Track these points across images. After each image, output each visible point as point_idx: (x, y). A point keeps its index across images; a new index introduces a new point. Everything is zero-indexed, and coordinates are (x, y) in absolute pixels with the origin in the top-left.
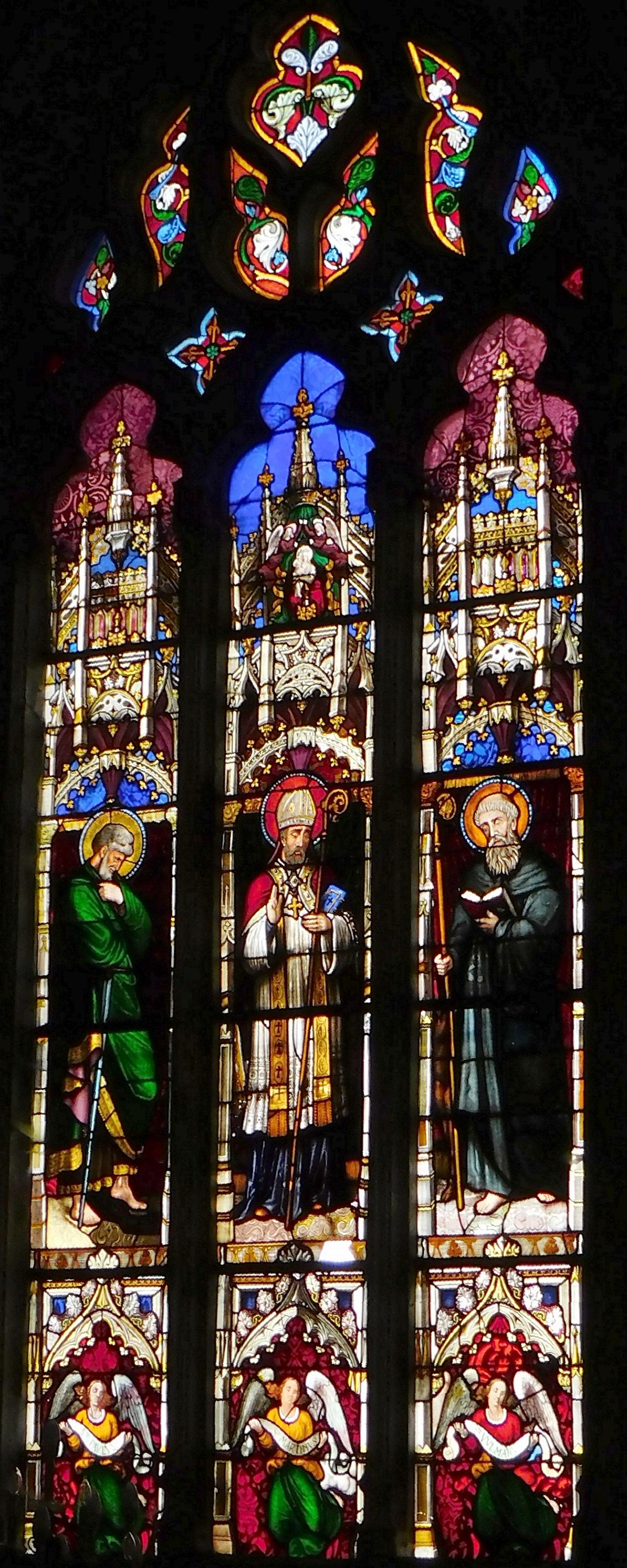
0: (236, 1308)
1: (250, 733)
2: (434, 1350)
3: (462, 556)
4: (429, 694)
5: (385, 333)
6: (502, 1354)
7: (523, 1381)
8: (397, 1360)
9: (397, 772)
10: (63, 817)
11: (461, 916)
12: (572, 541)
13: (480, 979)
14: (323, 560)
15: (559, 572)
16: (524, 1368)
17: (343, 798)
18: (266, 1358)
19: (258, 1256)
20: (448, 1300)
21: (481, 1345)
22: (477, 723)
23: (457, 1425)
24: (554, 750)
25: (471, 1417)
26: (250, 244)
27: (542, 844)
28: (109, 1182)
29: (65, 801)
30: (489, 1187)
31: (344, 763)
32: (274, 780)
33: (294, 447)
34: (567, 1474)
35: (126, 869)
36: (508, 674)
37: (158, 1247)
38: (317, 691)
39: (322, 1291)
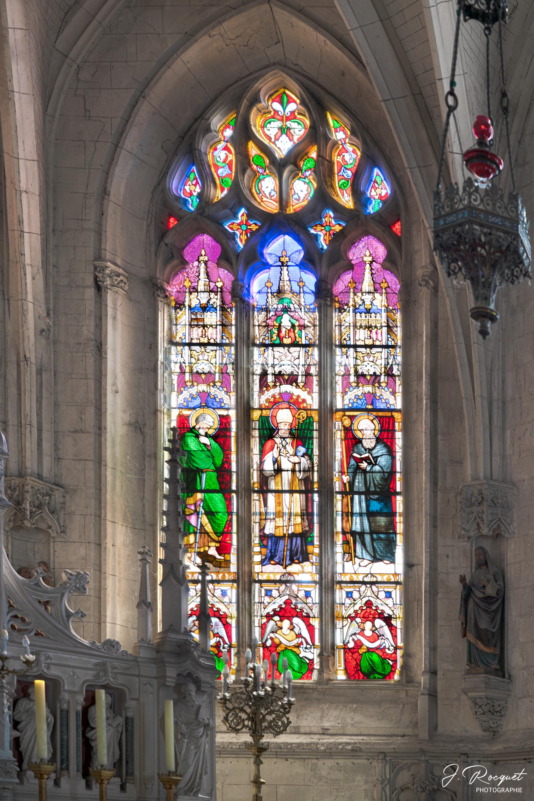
0: (263, 595)
1: (264, 385)
2: (344, 611)
3: (352, 328)
4: (339, 379)
5: (319, 233)
6: (369, 612)
7: (379, 622)
8: (330, 615)
9: (327, 411)
10: (182, 408)
11: (353, 462)
12: (395, 329)
13: (361, 485)
14: (294, 321)
15: (390, 339)
16: (379, 618)
17: (304, 414)
18: (276, 613)
19: (272, 577)
20: (349, 595)
21: (362, 610)
22: (359, 392)
23: (353, 636)
24: (389, 406)
25: (359, 634)
26: (260, 185)
27: (385, 437)
28: (207, 548)
29: (182, 402)
30: (365, 557)
31: (304, 401)
32: (274, 404)
33: (281, 273)
34: (395, 653)
35: (211, 432)
36: (371, 375)
37: (229, 573)
38: (292, 372)
39: (299, 590)
